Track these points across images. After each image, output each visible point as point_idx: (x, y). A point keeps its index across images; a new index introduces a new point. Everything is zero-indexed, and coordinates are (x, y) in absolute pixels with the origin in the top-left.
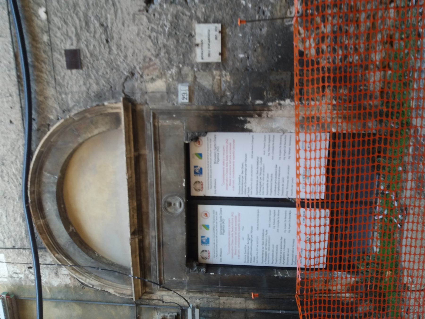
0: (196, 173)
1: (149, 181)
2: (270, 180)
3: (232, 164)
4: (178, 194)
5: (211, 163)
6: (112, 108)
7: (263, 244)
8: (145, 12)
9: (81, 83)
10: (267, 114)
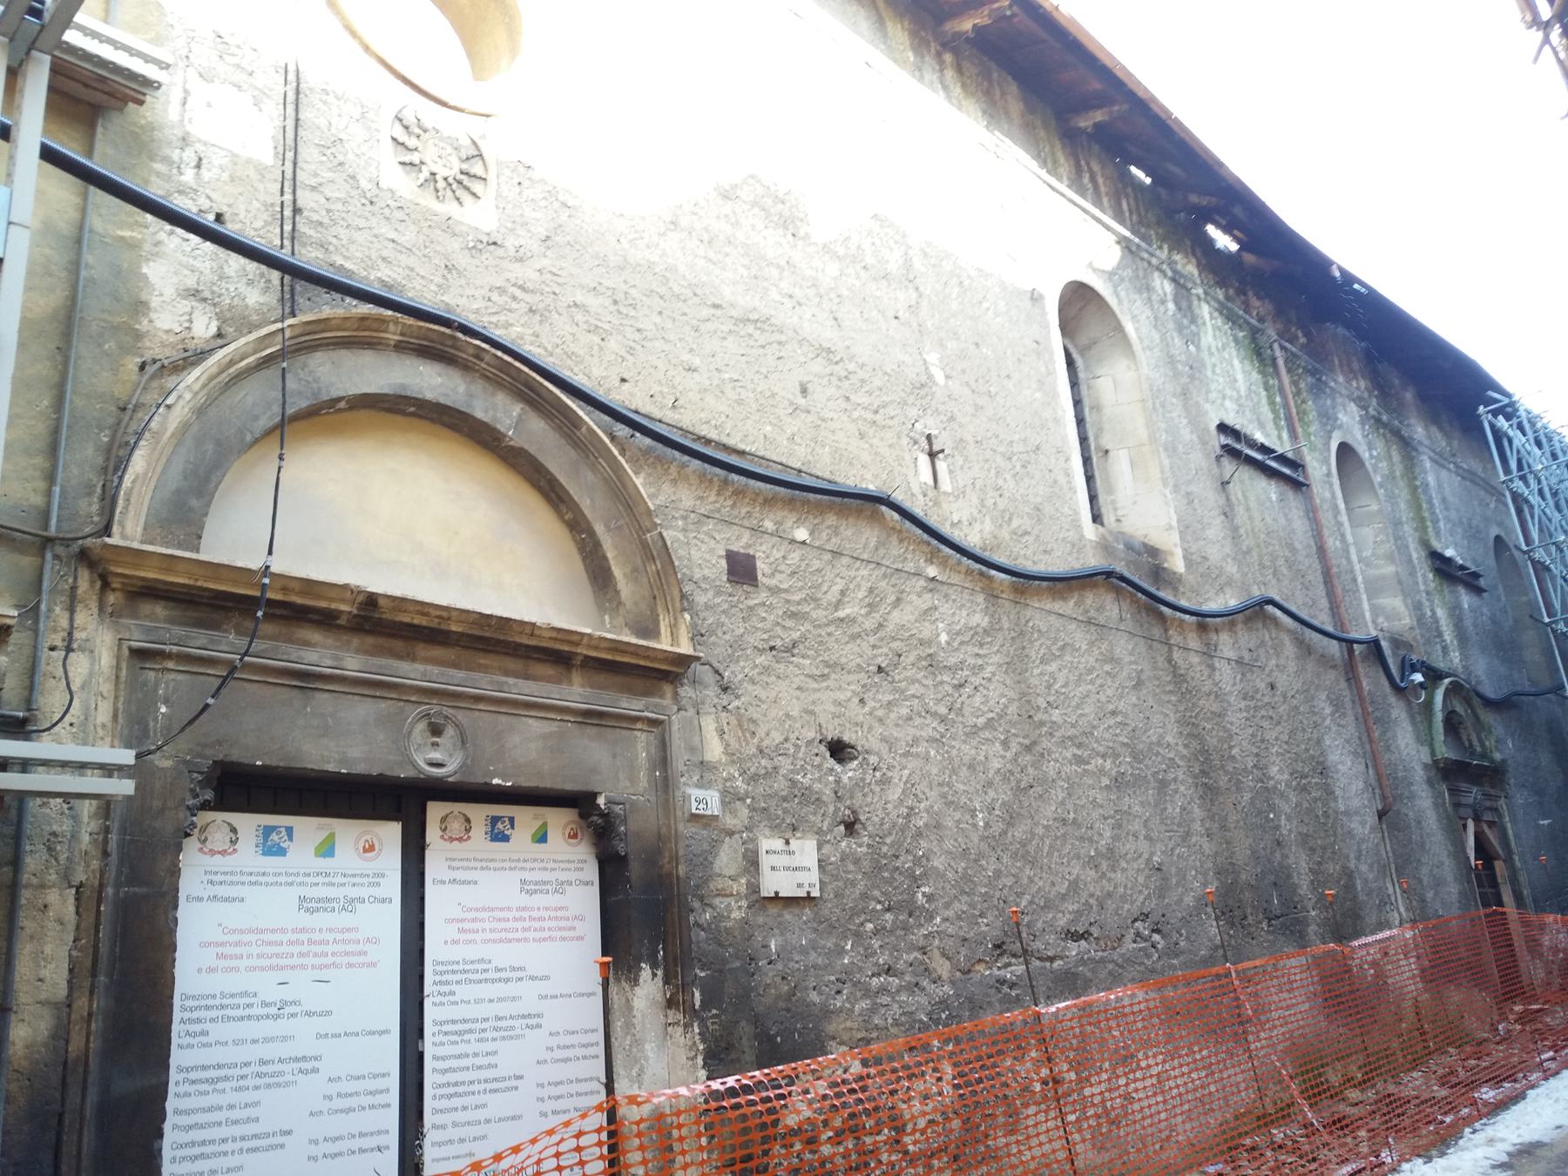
0: (495, 820)
1: (511, 681)
2: (479, 1061)
3: (520, 935)
4: (469, 762)
5: (522, 869)
6: (673, 628)
7: (263, 1062)
8: (819, 737)
9: (706, 572)
10: (677, 1023)
